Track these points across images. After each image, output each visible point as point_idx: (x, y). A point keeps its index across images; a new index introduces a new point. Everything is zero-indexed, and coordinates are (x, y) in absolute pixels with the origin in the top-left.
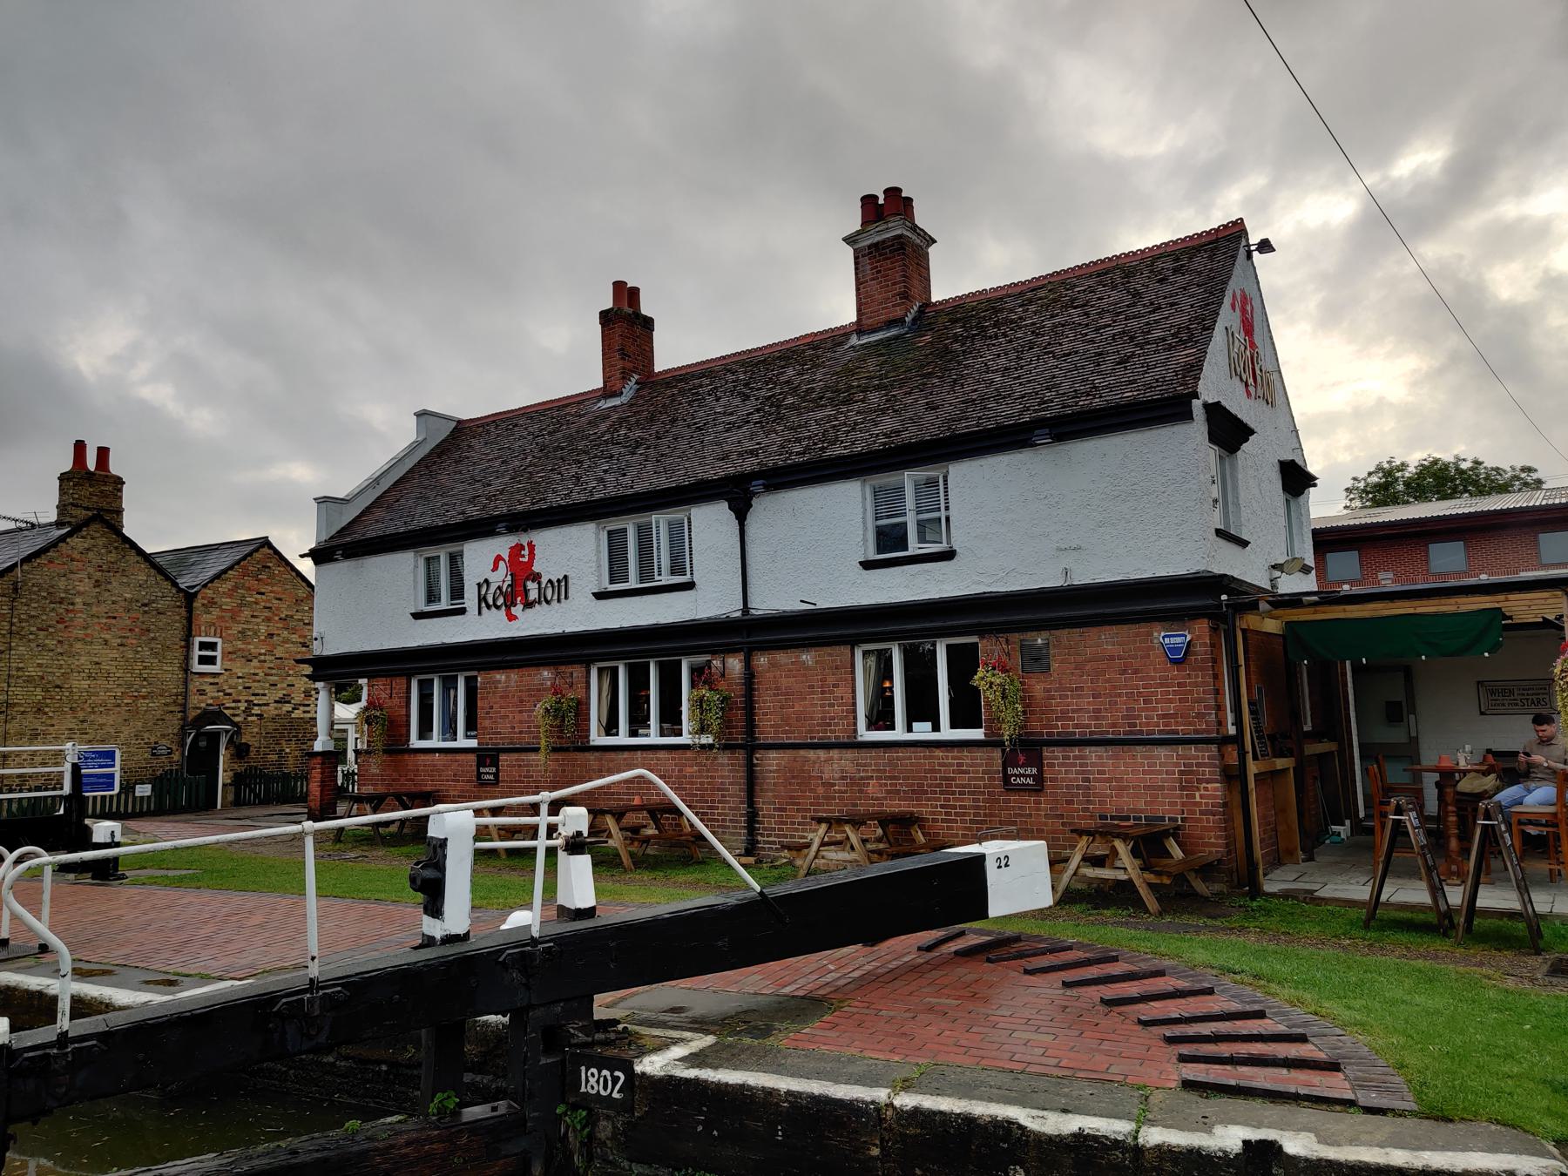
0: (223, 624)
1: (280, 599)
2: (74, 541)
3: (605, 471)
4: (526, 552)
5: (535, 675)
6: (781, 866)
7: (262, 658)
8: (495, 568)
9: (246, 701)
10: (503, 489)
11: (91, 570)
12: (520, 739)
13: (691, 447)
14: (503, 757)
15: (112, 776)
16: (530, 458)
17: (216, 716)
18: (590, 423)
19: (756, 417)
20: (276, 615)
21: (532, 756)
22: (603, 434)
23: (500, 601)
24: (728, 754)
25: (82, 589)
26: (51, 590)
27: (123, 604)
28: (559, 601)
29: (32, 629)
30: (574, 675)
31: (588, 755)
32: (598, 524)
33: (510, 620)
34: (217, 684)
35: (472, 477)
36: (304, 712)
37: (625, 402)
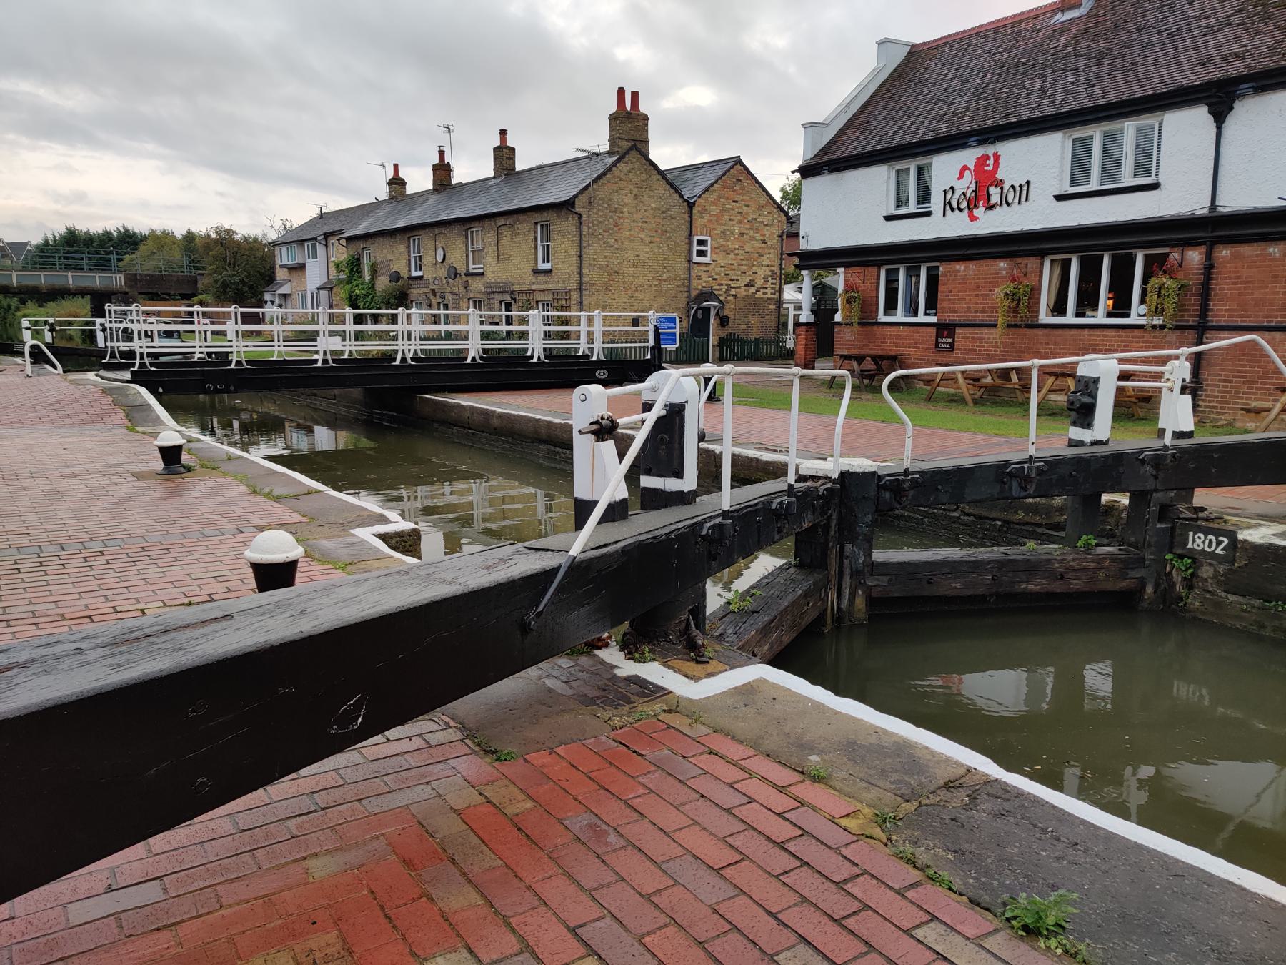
0: (711, 226)
1: (748, 206)
2: (621, 165)
3: (1072, 83)
4: (991, 162)
5: (992, 266)
6: (1223, 426)
7: (737, 252)
8: (961, 176)
9: (727, 285)
10: (968, 107)
11: (631, 187)
12: (975, 316)
13: (1164, 54)
14: (958, 330)
15: (674, 334)
16: (989, 76)
17: (709, 295)
18: (1048, 37)
19: (1238, 19)
20: (746, 218)
21: (993, 331)
22: (1064, 48)
23: (964, 205)
24: (1178, 333)
25: (626, 201)
26: (610, 203)
27: (651, 212)
28: (1019, 203)
29: (601, 231)
30: (1029, 266)
31: (1036, 331)
32: (1065, 133)
33: (971, 220)
34: (708, 271)
35: (935, 97)
36: (764, 293)
37: (1084, 14)
